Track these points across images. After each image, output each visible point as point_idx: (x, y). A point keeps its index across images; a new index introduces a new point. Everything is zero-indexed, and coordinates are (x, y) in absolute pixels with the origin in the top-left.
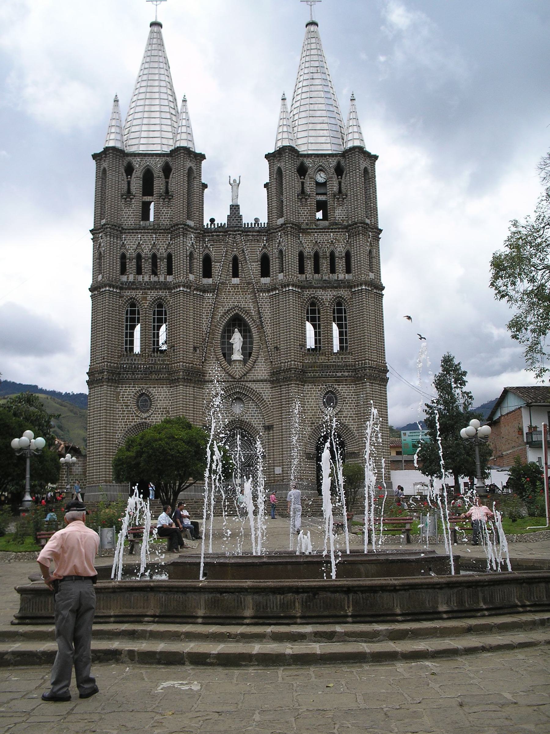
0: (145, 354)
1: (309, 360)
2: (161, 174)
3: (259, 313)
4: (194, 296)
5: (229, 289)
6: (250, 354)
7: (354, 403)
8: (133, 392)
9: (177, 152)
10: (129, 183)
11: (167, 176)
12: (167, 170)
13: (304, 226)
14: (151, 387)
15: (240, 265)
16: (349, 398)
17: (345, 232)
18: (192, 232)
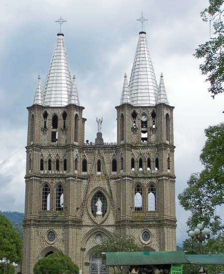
2: (62, 118)
3: (110, 190)
9: (70, 107)
11: (64, 119)
12: (65, 115)
13: (134, 145)
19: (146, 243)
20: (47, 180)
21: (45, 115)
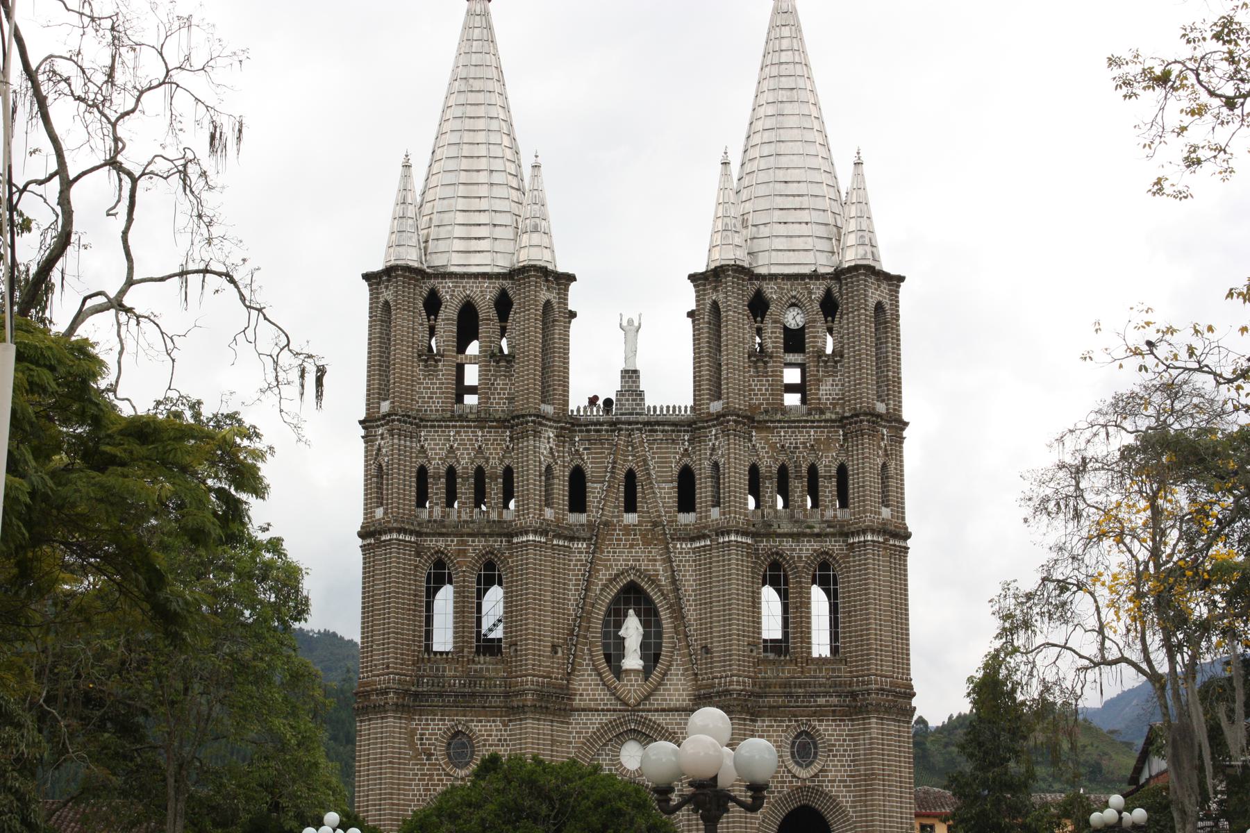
1: (766, 673)
2: (493, 313)
3: (674, 581)
5: (618, 535)
7: (849, 756)
14: (472, 721)
15: (639, 489)
16: (839, 745)
17: (838, 427)
19: (803, 773)
20: (441, 543)
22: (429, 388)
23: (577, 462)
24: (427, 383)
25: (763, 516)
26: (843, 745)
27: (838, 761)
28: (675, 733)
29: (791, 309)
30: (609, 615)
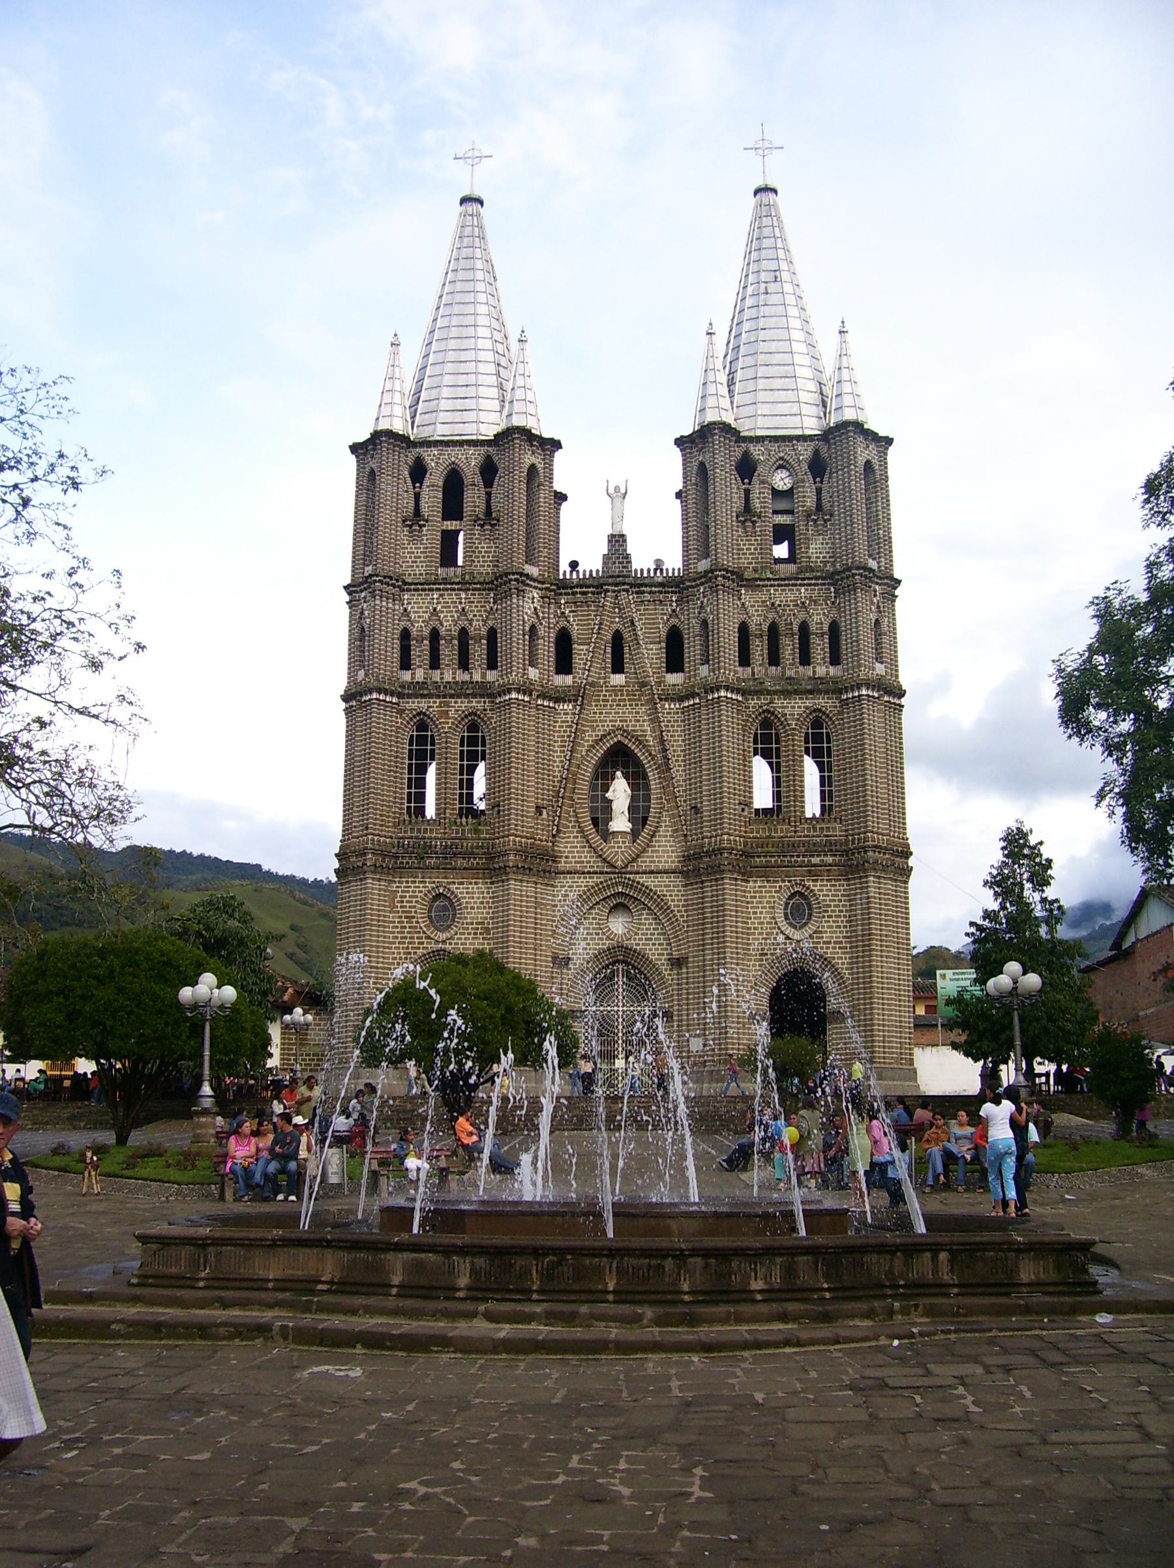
0: (445, 819)
2: (478, 479)
3: (662, 741)
4: (538, 710)
6: (644, 823)
7: (845, 916)
8: (421, 892)
10: (417, 497)
12: (489, 471)
14: (454, 883)
17: (829, 584)
18: (535, 588)
20: (422, 704)
21: (418, 472)
22: (413, 553)
23: (563, 623)
24: (411, 548)
25: (753, 673)
26: (838, 906)
27: (834, 922)
28: (664, 895)
29: (779, 471)
30: (597, 779)
